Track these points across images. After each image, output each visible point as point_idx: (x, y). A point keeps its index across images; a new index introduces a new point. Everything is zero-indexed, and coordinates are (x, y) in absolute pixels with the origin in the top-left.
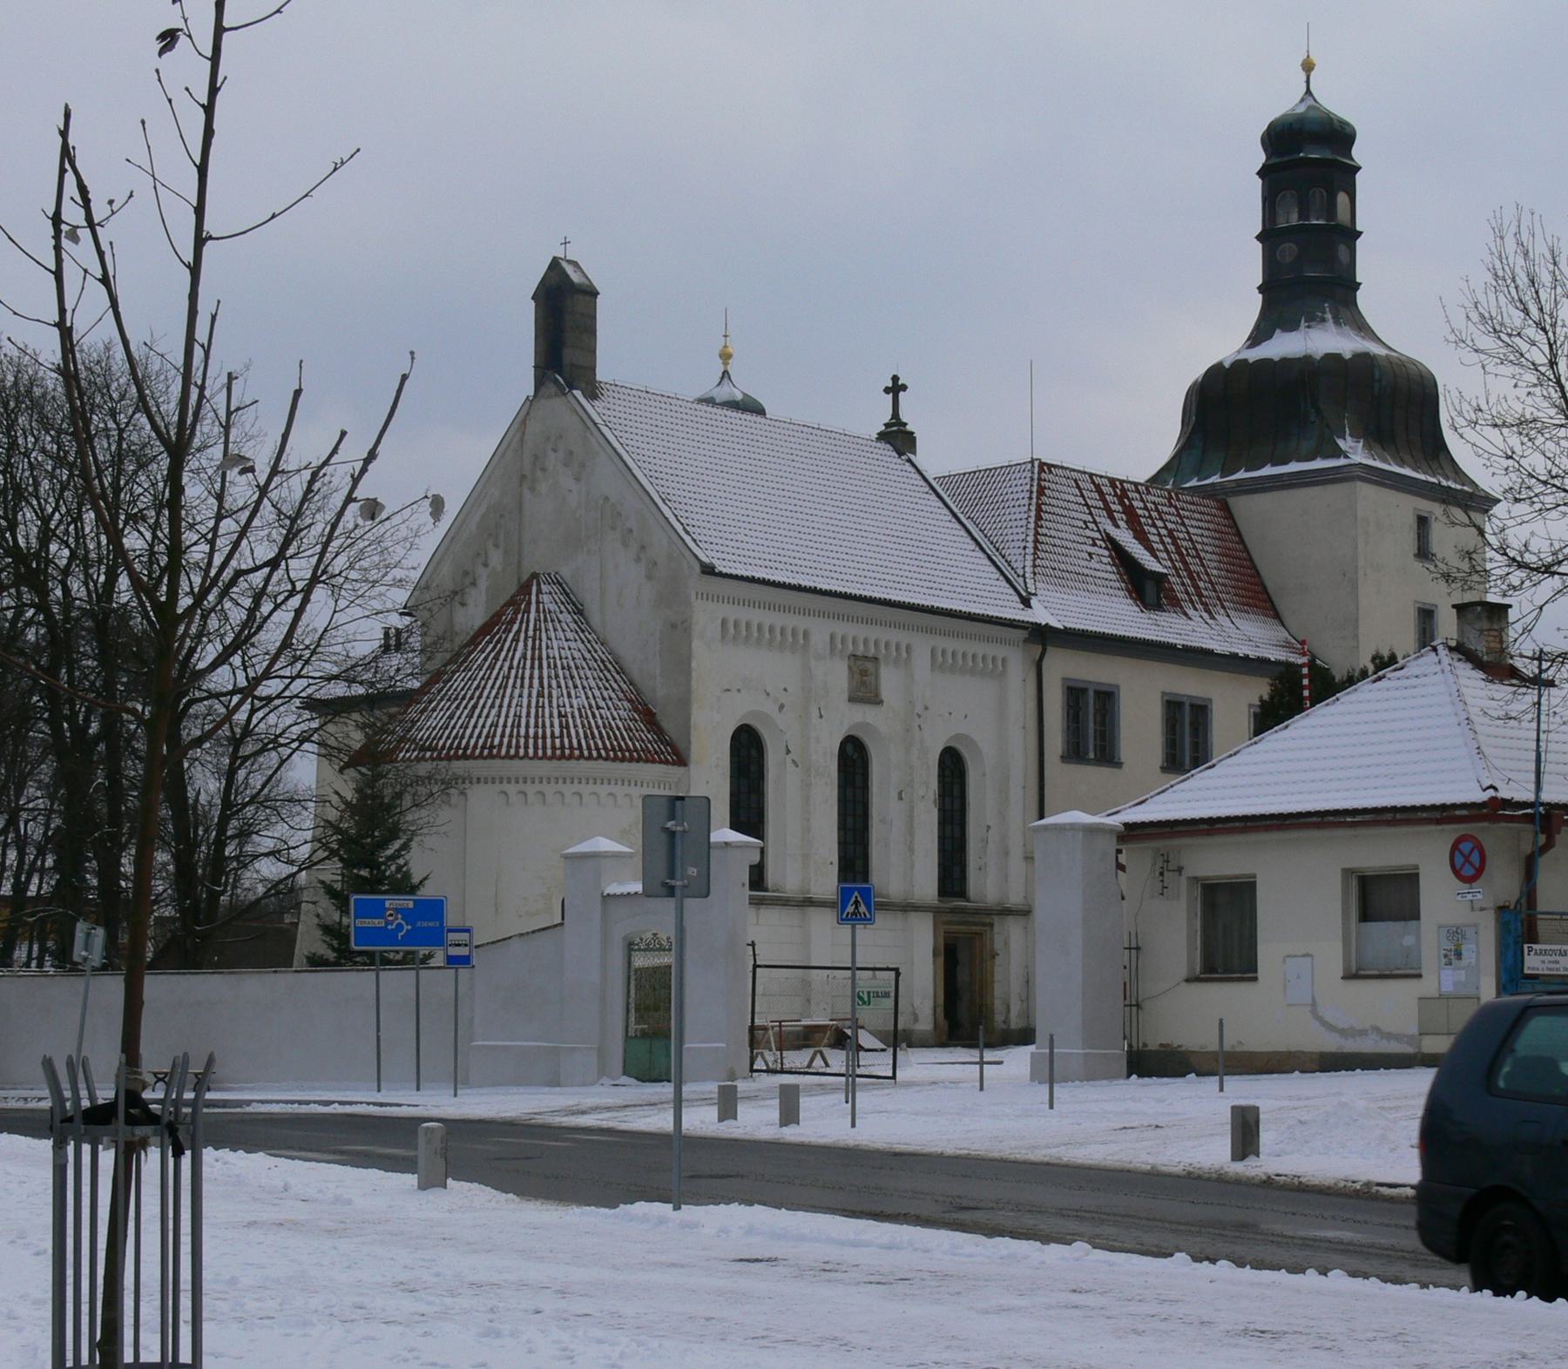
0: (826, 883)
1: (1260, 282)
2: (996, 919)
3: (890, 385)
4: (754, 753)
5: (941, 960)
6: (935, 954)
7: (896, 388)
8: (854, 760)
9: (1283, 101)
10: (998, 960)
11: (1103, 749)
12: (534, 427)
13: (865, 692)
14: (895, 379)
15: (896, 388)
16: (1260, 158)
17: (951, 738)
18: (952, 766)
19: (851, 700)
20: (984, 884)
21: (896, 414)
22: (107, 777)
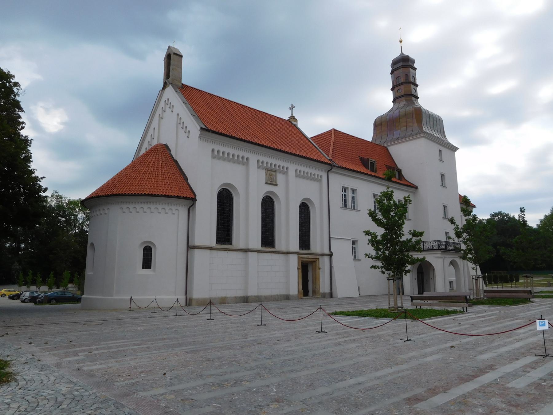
2: (320, 257)
5: (301, 270)
6: (298, 269)
8: (268, 205)
9: (396, 54)
10: (321, 271)
11: (354, 206)
13: (271, 181)
14: (292, 105)
18: (305, 210)
19: (266, 183)
20: (318, 244)
21: (292, 114)
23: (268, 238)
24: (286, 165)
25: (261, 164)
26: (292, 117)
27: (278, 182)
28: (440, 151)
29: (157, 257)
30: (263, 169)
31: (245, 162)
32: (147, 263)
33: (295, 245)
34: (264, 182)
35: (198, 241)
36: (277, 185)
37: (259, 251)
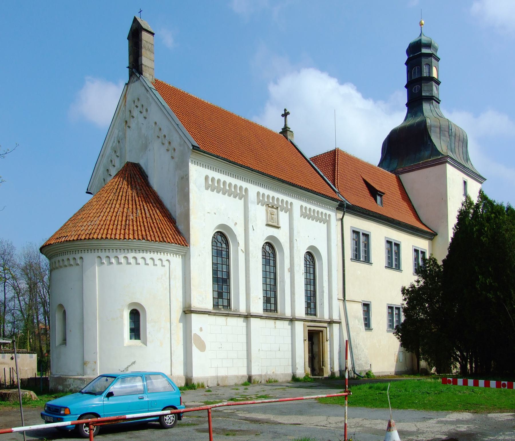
0: (258, 307)
1: (406, 102)
3: (284, 113)
4: (224, 246)
7: (285, 115)
9: (413, 38)
12: (129, 98)
15: (285, 115)
16: (406, 58)
17: (308, 249)
18: (311, 257)
19: (268, 225)
21: (285, 125)
22: (421, 319)
23: (271, 301)
24: (290, 199)
25: (210, 183)
26: (285, 131)
27: (281, 225)
28: (465, 183)
29: (150, 325)
30: (263, 205)
31: (243, 195)
32: (136, 332)
33: (301, 311)
34: (265, 223)
35: (196, 304)
36: (278, 228)
37: (260, 317)
